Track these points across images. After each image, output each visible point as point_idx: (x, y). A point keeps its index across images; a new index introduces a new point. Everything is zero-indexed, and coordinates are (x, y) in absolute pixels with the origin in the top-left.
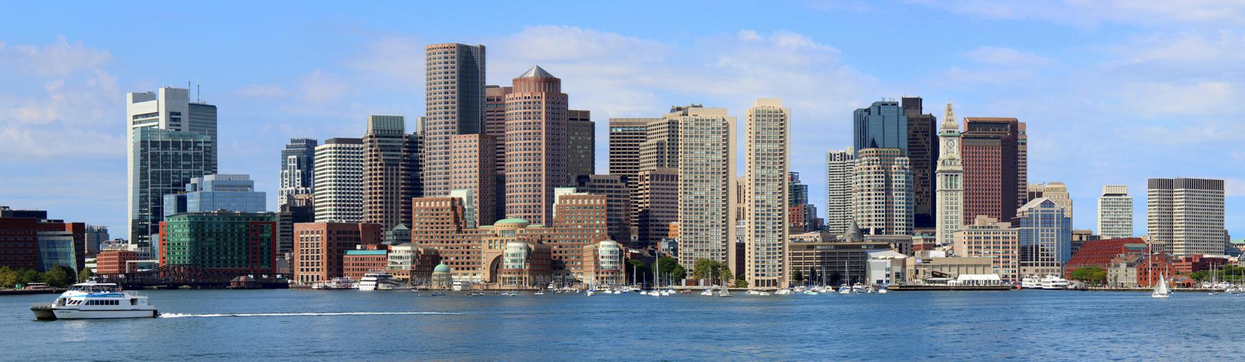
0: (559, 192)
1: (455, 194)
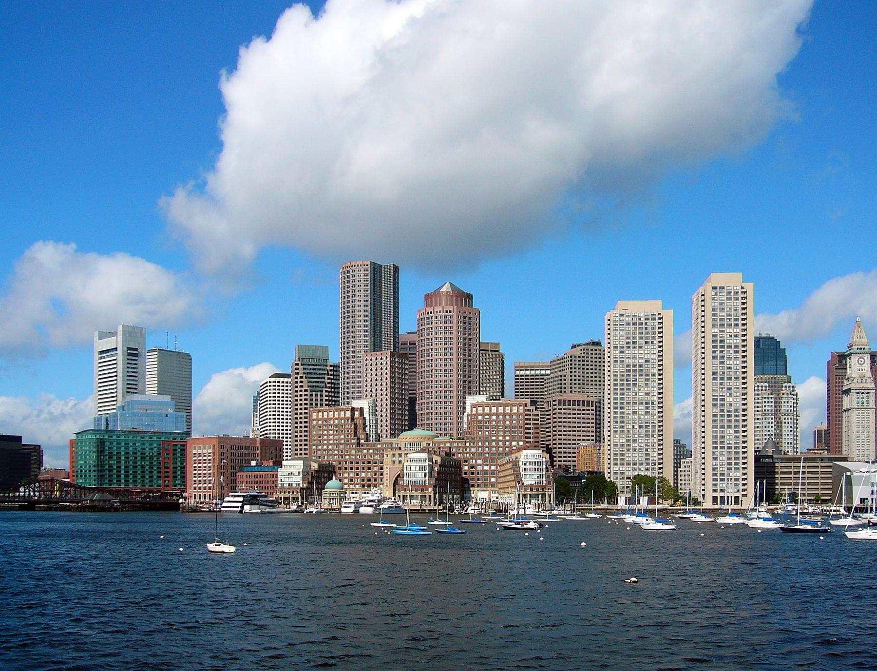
0: (470, 400)
1: (356, 404)
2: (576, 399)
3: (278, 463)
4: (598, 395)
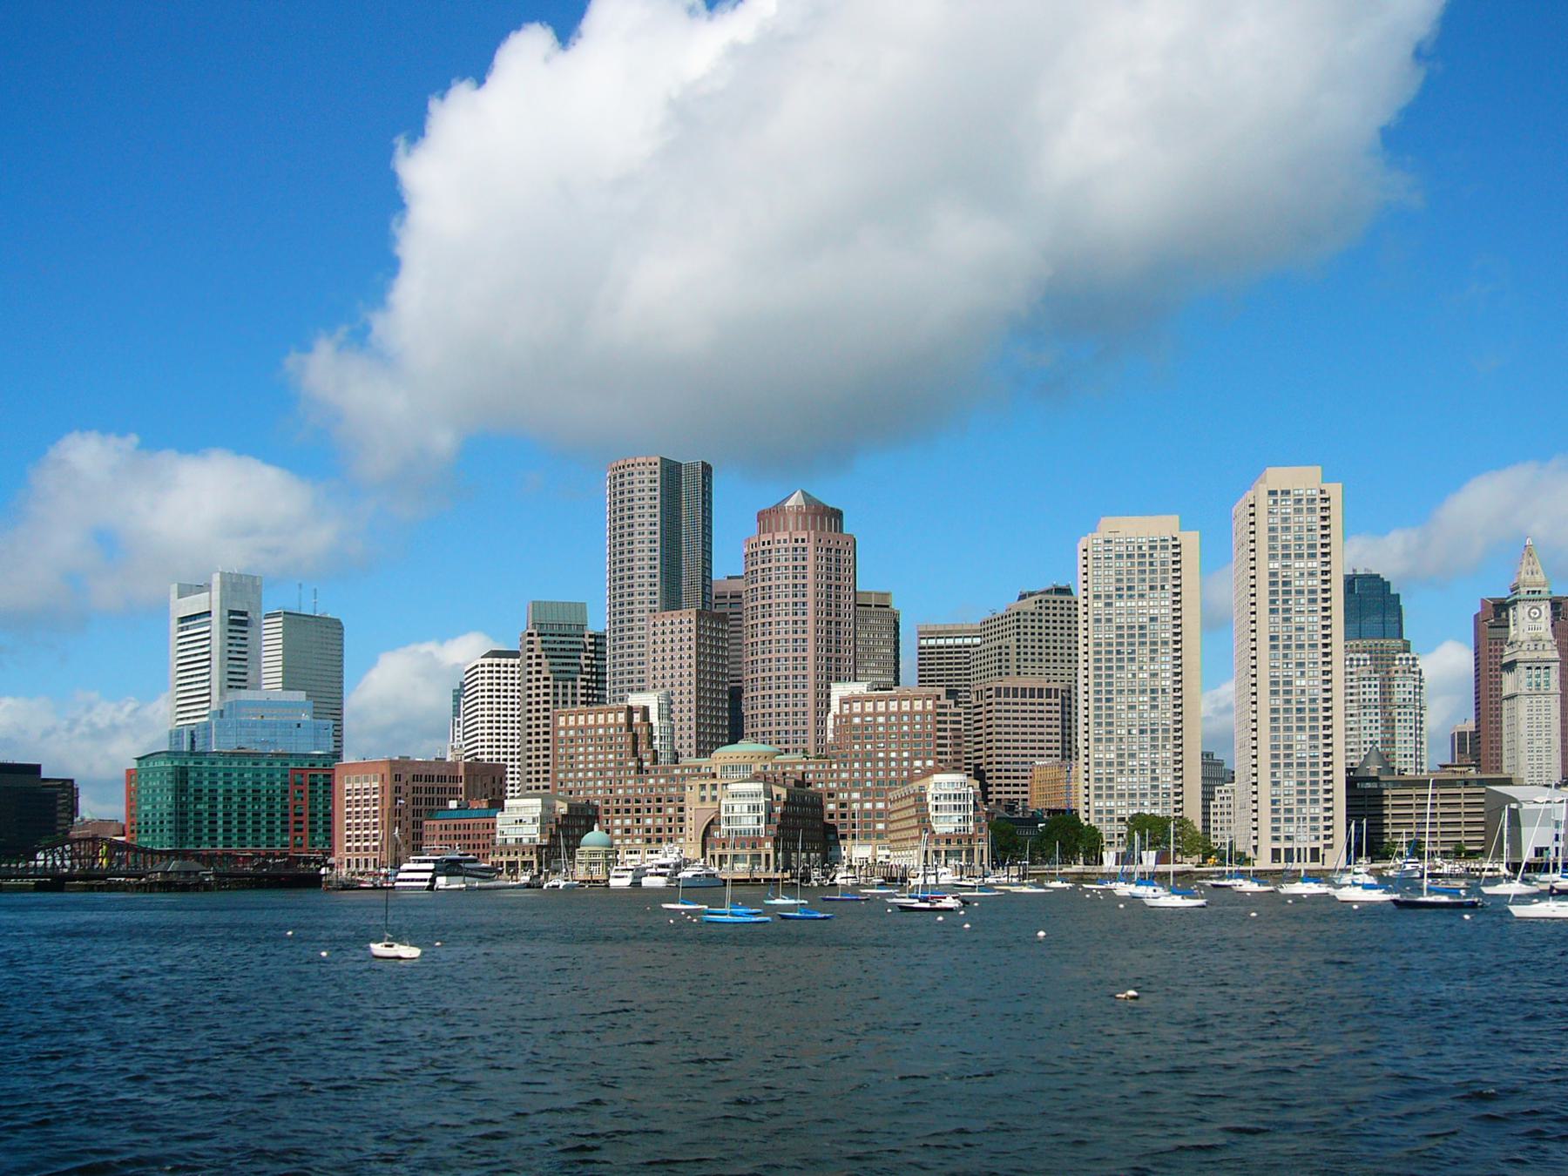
0: (839, 691)
1: (635, 700)
2: (1028, 686)
3: (497, 804)
4: (1066, 678)
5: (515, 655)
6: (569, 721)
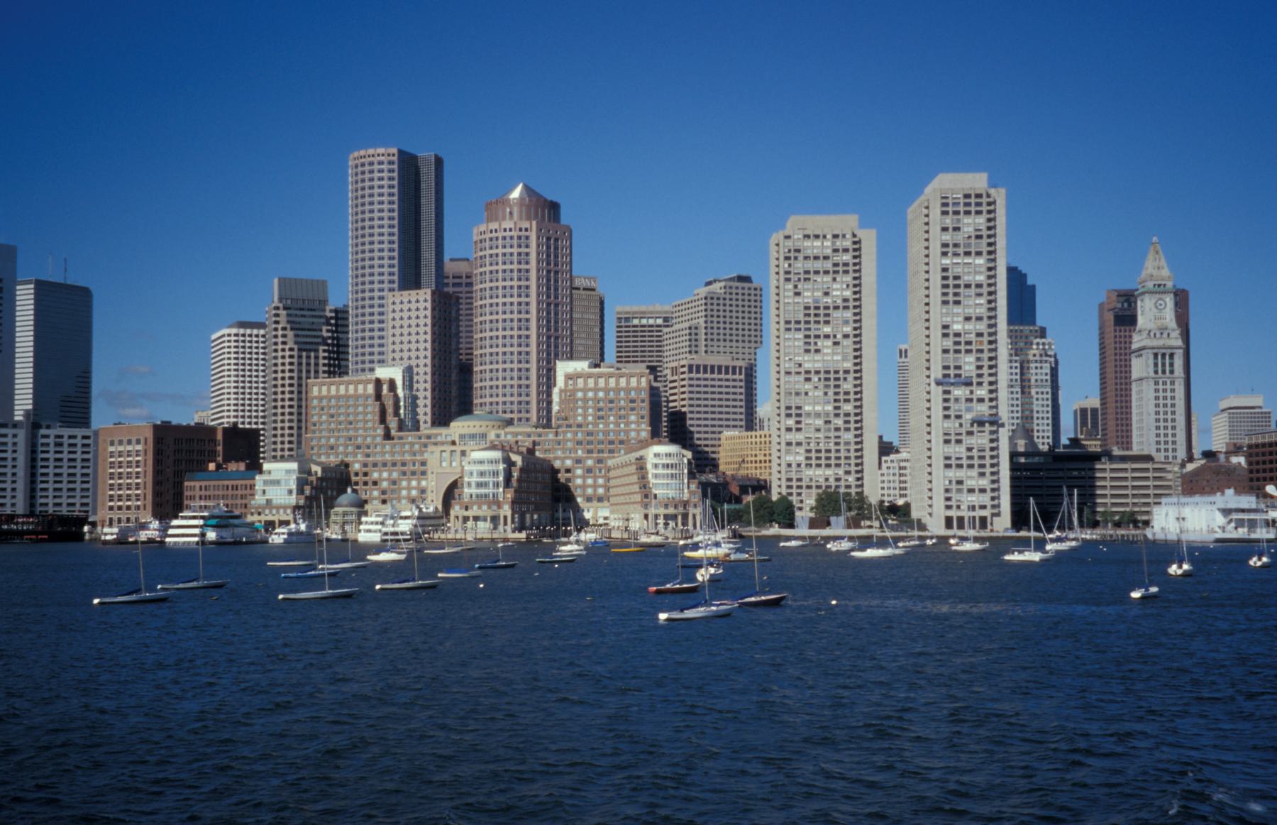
0: (563, 368)
1: (382, 373)
2: (716, 363)
3: (255, 467)
4: (747, 356)
5: (261, 325)
6: (321, 389)
